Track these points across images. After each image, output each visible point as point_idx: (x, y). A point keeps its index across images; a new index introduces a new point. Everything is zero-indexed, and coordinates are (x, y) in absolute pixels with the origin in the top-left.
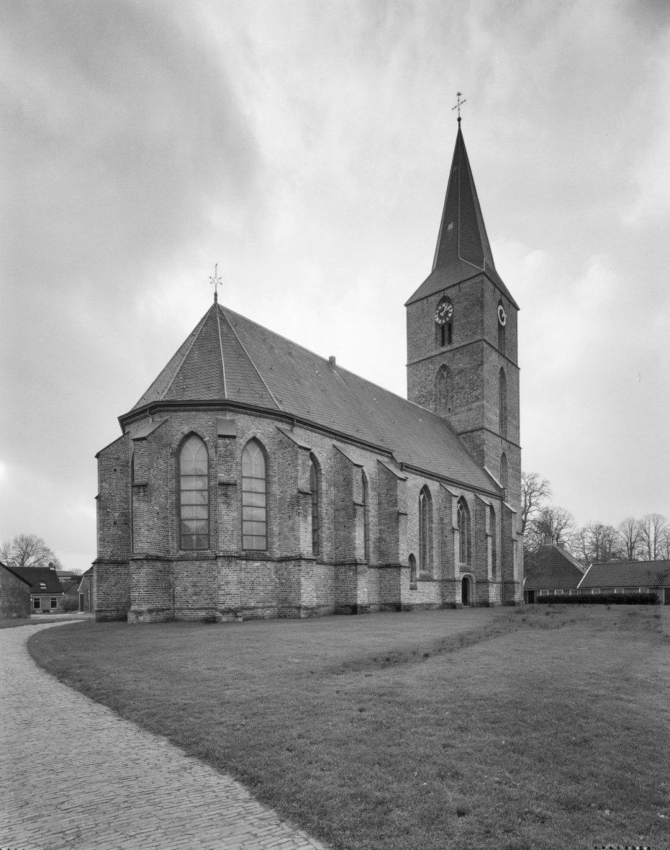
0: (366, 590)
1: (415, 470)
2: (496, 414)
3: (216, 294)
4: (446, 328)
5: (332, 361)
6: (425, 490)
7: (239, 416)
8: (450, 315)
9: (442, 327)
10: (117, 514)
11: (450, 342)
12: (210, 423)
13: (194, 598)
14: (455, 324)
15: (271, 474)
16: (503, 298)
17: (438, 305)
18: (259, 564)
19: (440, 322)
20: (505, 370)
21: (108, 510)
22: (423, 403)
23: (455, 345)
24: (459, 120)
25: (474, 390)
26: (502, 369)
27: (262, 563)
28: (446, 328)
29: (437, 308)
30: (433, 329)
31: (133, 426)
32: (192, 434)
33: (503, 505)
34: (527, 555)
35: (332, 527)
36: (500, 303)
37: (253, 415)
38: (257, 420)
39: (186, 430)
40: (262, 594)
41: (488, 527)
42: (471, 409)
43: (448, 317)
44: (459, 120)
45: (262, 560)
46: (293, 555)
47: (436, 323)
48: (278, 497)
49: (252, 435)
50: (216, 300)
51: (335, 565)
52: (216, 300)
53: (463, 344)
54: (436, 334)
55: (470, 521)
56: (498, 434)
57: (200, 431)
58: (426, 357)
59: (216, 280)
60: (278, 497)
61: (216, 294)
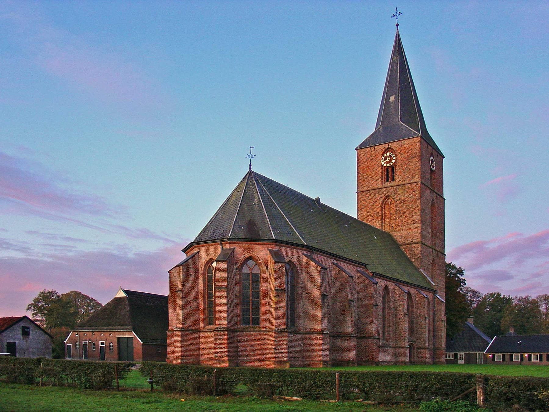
0: (355, 352)
1: (358, 264)
2: (428, 232)
3: (250, 165)
4: (390, 169)
5: (318, 200)
6: (386, 287)
7: (282, 248)
8: (393, 161)
9: (387, 168)
10: (192, 302)
11: (393, 179)
12: (263, 252)
13: (252, 354)
14: (398, 169)
15: (300, 282)
16: (434, 152)
17: (384, 153)
18: (293, 335)
19: (385, 165)
20: (435, 201)
21: (187, 299)
22: (371, 220)
23: (398, 183)
24: (397, 25)
25: (413, 216)
26: (433, 200)
27: (294, 334)
28: (390, 169)
29: (383, 155)
30: (380, 170)
31: (203, 248)
32: (250, 258)
33: (434, 296)
34: (53, 358)
35: (332, 313)
36: (432, 155)
37: (290, 248)
38: (292, 250)
39: (247, 255)
40: (293, 353)
41: (426, 312)
42: (410, 229)
43: (392, 163)
44: (397, 25)
45: (294, 333)
46: (316, 331)
47: (382, 166)
48: (303, 296)
49: (289, 259)
50: (250, 168)
51: (333, 336)
52: (250, 168)
53: (404, 182)
54: (382, 173)
55: (413, 308)
56: (430, 245)
57: (257, 256)
58: (373, 188)
59: (251, 156)
60: (303, 296)
61: (250, 165)
